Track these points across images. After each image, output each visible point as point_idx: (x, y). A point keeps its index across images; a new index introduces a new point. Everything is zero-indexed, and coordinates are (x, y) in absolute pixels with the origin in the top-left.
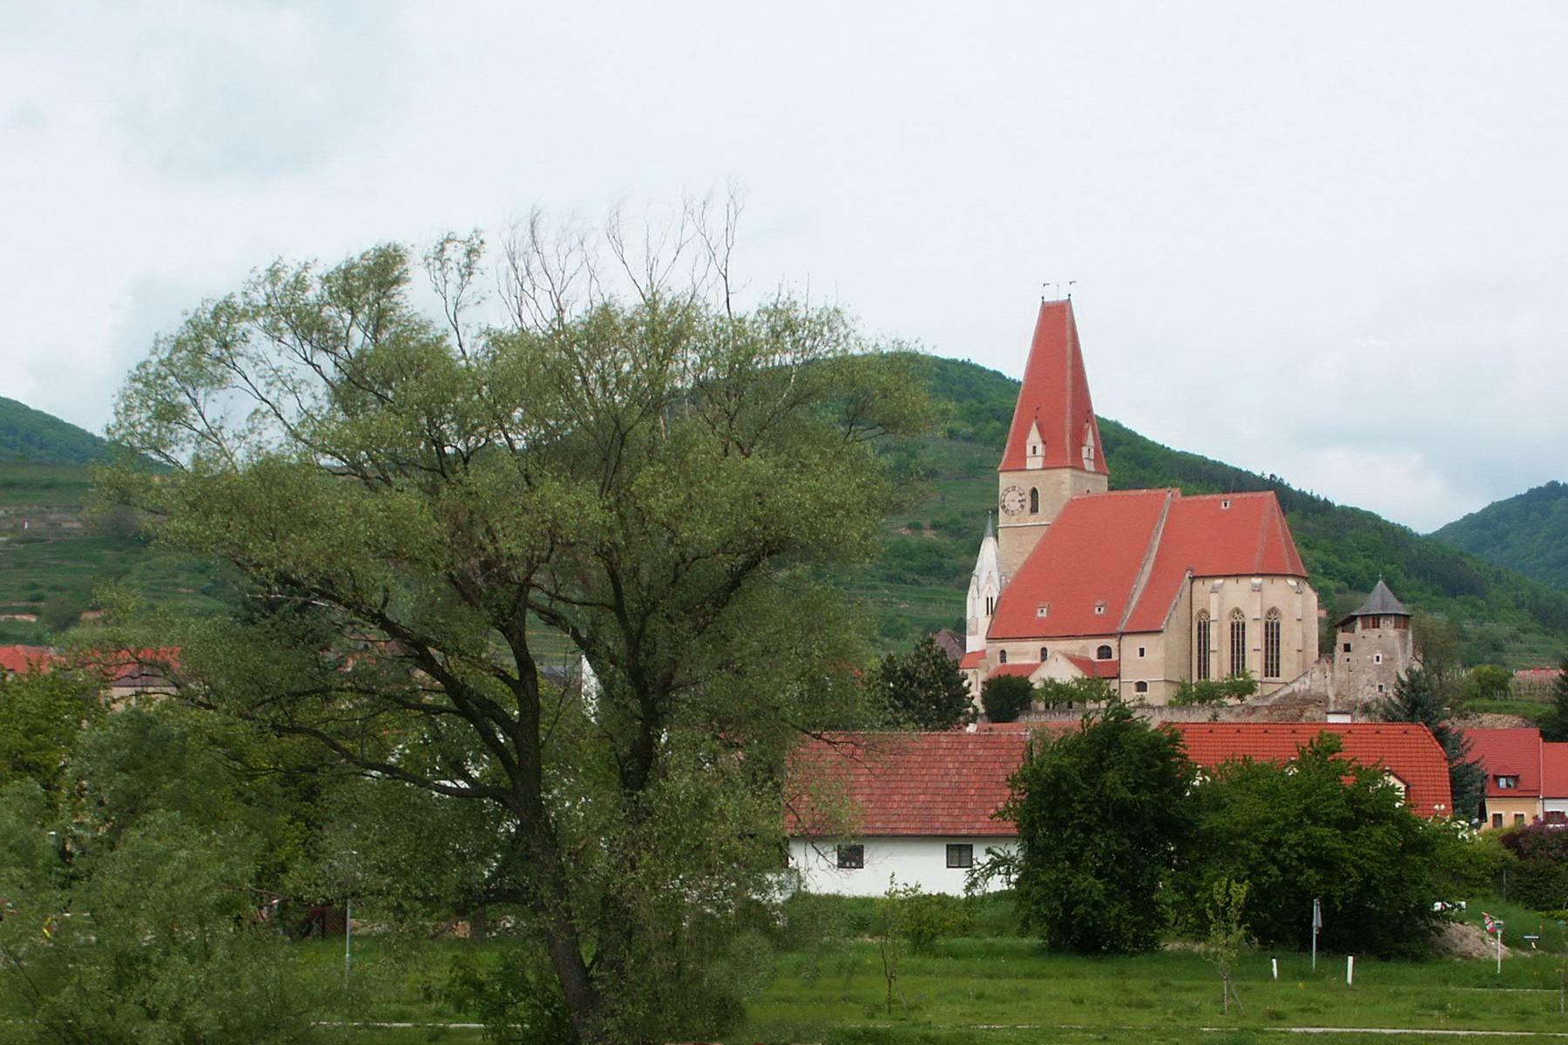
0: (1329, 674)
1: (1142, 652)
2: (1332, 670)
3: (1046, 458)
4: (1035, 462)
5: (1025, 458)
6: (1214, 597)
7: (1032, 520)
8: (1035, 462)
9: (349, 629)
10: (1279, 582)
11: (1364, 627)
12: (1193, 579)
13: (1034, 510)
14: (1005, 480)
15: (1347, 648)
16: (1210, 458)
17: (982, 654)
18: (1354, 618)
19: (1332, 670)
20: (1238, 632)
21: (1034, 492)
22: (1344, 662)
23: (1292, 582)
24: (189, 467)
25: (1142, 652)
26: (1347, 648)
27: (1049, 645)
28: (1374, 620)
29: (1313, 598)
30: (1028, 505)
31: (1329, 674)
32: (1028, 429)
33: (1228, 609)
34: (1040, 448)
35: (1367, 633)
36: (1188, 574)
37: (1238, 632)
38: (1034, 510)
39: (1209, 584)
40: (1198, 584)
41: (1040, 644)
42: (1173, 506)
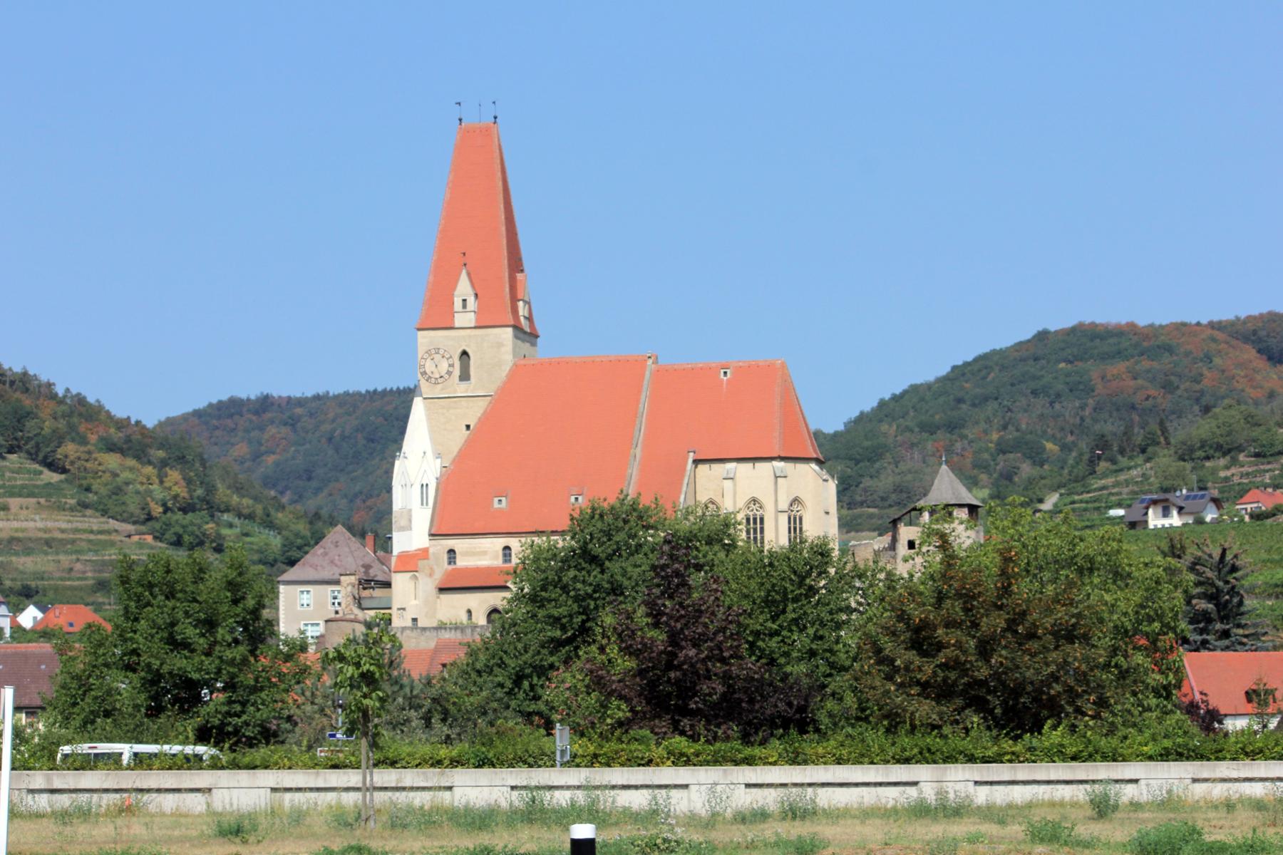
4: (465, 319)
6: (728, 484)
7: (462, 389)
8: (465, 319)
13: (465, 376)
17: (424, 553)
23: (814, 466)
27: (458, 544)
30: (457, 372)
38: (465, 376)
40: (702, 468)
41: (501, 542)
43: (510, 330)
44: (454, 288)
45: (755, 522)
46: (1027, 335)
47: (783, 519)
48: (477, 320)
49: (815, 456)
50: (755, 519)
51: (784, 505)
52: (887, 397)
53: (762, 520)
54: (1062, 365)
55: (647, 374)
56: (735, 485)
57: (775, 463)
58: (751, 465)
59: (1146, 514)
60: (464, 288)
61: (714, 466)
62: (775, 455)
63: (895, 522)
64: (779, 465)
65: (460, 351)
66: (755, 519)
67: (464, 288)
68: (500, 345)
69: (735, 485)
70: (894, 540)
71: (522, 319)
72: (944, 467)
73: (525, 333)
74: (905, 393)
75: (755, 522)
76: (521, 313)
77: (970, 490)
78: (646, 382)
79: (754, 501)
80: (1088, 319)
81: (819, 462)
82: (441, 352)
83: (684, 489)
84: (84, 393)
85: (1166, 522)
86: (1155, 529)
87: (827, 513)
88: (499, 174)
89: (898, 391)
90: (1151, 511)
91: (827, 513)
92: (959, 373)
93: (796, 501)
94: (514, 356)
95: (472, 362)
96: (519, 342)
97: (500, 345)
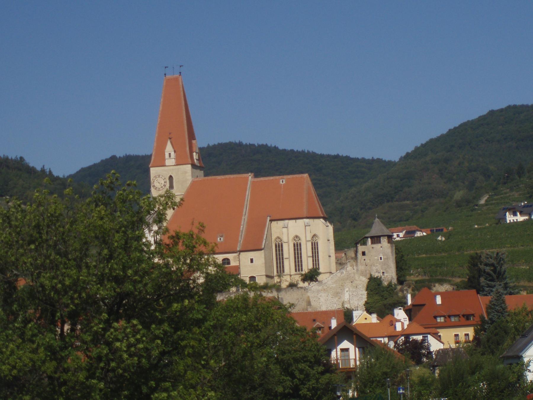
0: (355, 268)
1: (252, 261)
2: (357, 265)
3: (177, 158)
4: (170, 161)
5: (164, 160)
6: (285, 230)
8: (170, 161)
9: (308, 363)
10: (316, 221)
11: (372, 243)
12: (271, 221)
14: (153, 171)
15: (364, 254)
16: (318, 152)
18: (367, 238)
19: (357, 265)
20: (297, 247)
21: (171, 177)
22: (363, 261)
23: (322, 220)
24: (48, 173)
25: (252, 261)
26: (364, 254)
28: (376, 239)
29: (331, 228)
31: (355, 268)
32: (166, 144)
33: (291, 237)
34: (173, 154)
35: (374, 246)
36: (269, 219)
37: (297, 247)
39: (281, 223)
40: (274, 223)
42: (253, 183)
43: (190, 166)
44: (165, 148)
45: (297, 246)
46: (484, 112)
47: (309, 245)
48: (176, 162)
49: (322, 216)
50: (297, 245)
51: (309, 238)
52: (419, 145)
53: (300, 244)
54: (500, 127)
55: (249, 183)
56: (288, 230)
57: (305, 220)
58: (294, 221)
59: (505, 215)
60: (169, 148)
61: (279, 222)
62: (305, 216)
63: (356, 244)
64: (306, 221)
65: (169, 176)
66: (297, 245)
67: (169, 148)
68: (186, 172)
69: (288, 230)
70: (356, 252)
71: (195, 160)
72: (377, 219)
73: (197, 166)
74: (427, 143)
75: (297, 246)
76: (195, 158)
77: (388, 228)
78: (248, 186)
79: (297, 237)
80: (512, 103)
81: (324, 218)
82: (161, 176)
83: (266, 233)
84: (35, 166)
85: (515, 218)
86: (510, 223)
87: (329, 240)
88: (183, 98)
89: (424, 142)
90: (507, 214)
91: (329, 240)
92: (452, 133)
93: (315, 236)
94: (192, 177)
95: (174, 180)
96: (194, 170)
97: (186, 172)
